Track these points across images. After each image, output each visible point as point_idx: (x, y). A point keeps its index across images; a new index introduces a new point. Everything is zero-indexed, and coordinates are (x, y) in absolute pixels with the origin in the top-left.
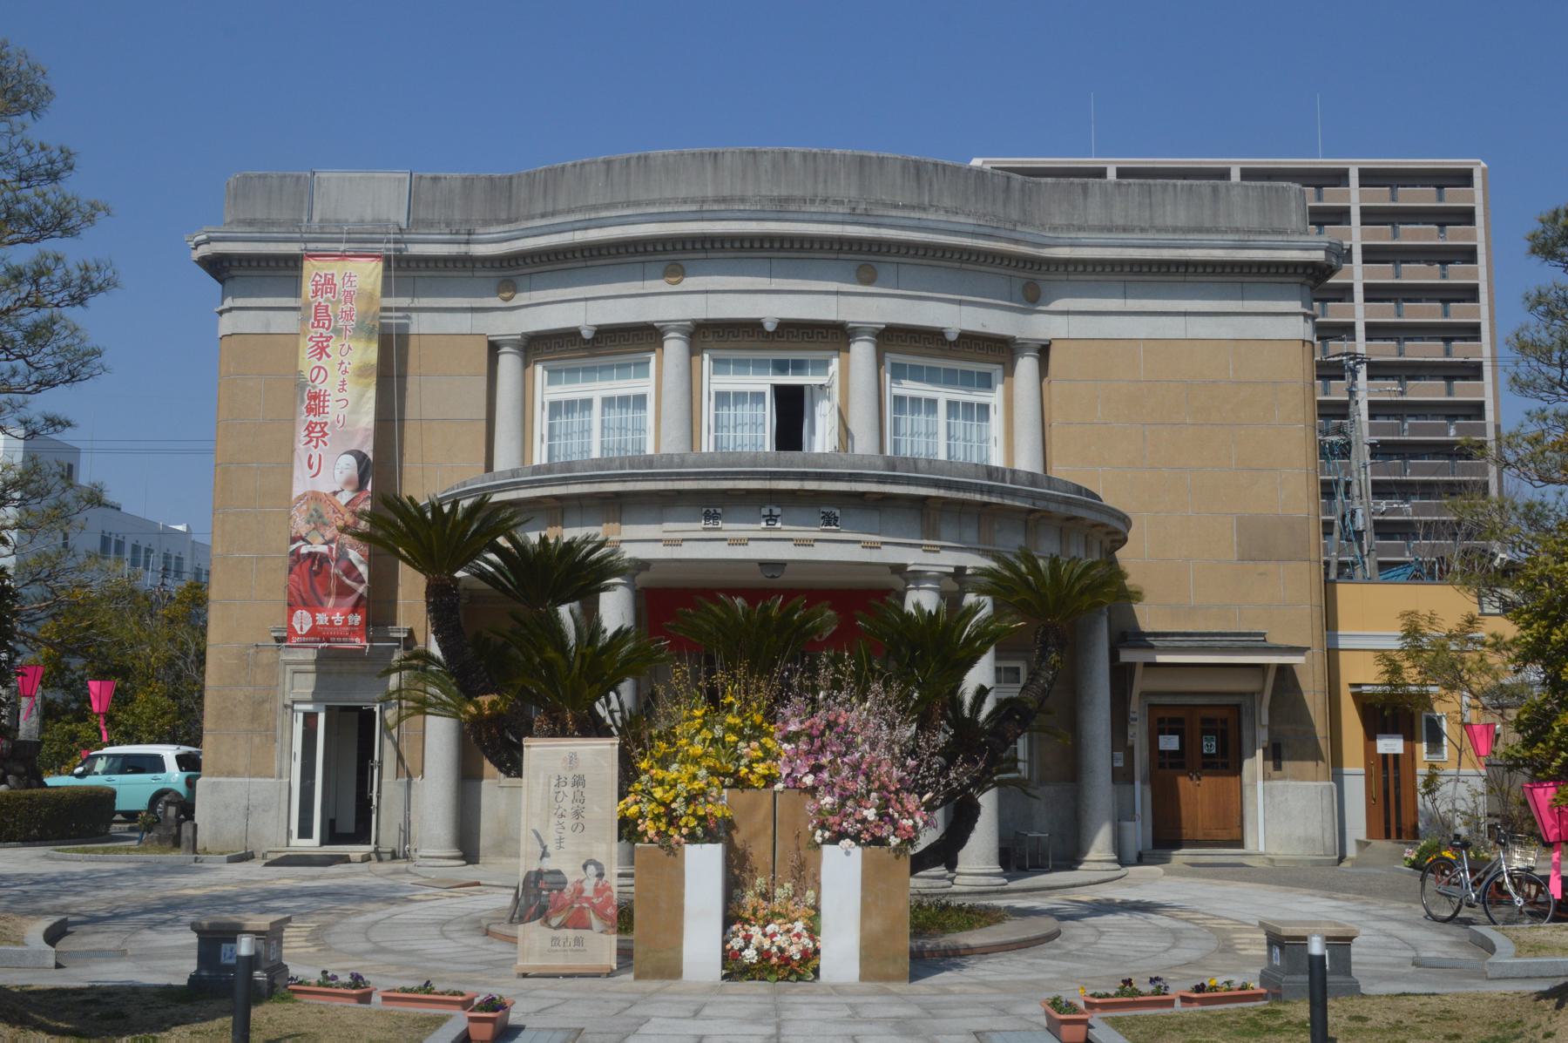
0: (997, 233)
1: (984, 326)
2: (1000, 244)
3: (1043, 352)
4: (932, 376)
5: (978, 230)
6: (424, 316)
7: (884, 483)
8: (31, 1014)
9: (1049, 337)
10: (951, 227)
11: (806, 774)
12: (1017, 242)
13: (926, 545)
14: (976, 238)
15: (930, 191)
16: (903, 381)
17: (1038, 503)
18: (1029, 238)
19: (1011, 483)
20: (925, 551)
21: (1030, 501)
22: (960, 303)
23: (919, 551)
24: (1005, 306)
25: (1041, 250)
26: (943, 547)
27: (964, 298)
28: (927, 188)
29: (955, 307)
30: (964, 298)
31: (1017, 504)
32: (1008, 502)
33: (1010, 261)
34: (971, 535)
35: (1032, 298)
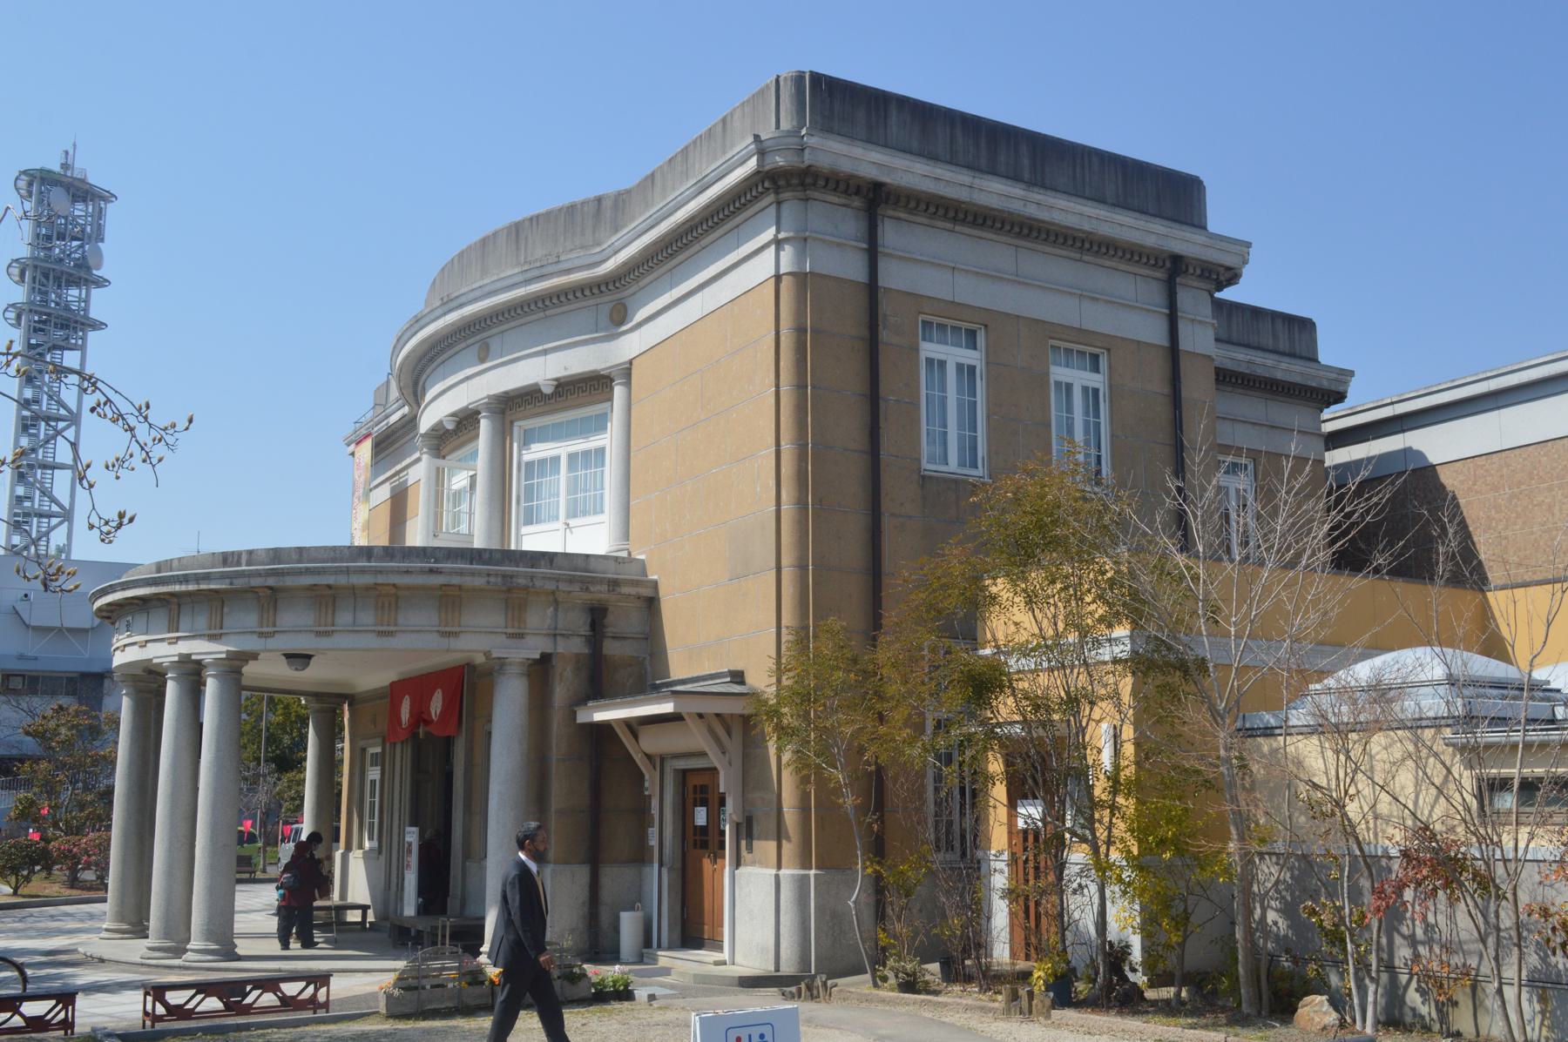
0: (545, 271)
1: (566, 369)
2: (551, 281)
3: (627, 371)
4: (556, 437)
5: (529, 275)
6: (411, 470)
7: (129, 588)
8: (294, 931)
9: (626, 359)
10: (505, 283)
11: (1378, 753)
12: (568, 271)
13: (169, 639)
14: (530, 285)
15: (525, 251)
16: (532, 446)
17: (235, 581)
18: (577, 263)
19: (247, 565)
20: (169, 643)
21: (228, 581)
22: (545, 352)
23: (165, 644)
24: (592, 339)
25: (596, 270)
26: (178, 638)
27: (546, 346)
28: (523, 251)
29: (541, 359)
30: (546, 346)
31: (213, 587)
32: (203, 587)
33: (1021, 228)
34: (201, 622)
35: (619, 318)
